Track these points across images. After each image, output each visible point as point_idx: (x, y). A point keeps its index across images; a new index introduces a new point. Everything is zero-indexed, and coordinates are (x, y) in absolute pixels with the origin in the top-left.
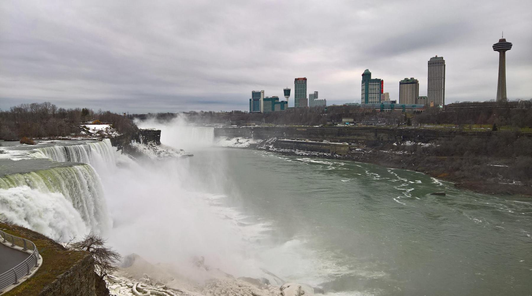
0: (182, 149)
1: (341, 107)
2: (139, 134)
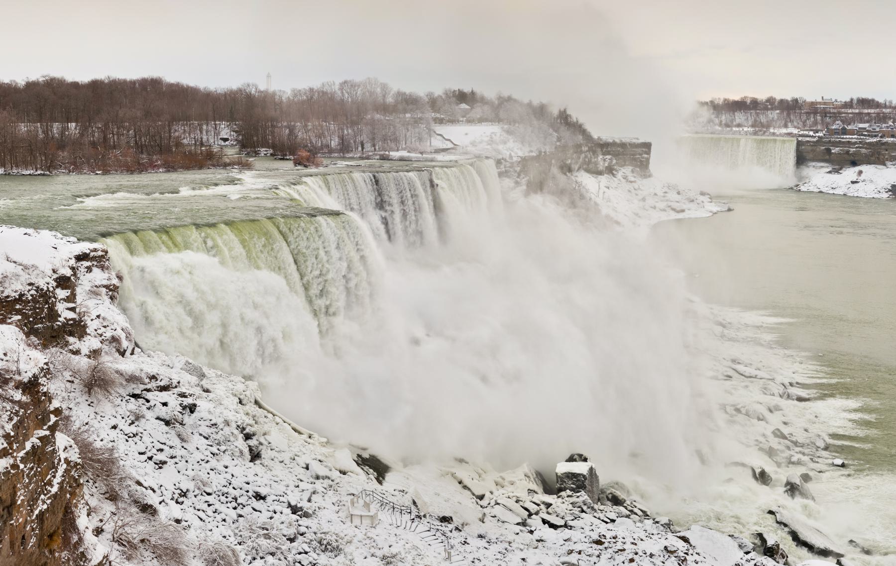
1: (133, 83)
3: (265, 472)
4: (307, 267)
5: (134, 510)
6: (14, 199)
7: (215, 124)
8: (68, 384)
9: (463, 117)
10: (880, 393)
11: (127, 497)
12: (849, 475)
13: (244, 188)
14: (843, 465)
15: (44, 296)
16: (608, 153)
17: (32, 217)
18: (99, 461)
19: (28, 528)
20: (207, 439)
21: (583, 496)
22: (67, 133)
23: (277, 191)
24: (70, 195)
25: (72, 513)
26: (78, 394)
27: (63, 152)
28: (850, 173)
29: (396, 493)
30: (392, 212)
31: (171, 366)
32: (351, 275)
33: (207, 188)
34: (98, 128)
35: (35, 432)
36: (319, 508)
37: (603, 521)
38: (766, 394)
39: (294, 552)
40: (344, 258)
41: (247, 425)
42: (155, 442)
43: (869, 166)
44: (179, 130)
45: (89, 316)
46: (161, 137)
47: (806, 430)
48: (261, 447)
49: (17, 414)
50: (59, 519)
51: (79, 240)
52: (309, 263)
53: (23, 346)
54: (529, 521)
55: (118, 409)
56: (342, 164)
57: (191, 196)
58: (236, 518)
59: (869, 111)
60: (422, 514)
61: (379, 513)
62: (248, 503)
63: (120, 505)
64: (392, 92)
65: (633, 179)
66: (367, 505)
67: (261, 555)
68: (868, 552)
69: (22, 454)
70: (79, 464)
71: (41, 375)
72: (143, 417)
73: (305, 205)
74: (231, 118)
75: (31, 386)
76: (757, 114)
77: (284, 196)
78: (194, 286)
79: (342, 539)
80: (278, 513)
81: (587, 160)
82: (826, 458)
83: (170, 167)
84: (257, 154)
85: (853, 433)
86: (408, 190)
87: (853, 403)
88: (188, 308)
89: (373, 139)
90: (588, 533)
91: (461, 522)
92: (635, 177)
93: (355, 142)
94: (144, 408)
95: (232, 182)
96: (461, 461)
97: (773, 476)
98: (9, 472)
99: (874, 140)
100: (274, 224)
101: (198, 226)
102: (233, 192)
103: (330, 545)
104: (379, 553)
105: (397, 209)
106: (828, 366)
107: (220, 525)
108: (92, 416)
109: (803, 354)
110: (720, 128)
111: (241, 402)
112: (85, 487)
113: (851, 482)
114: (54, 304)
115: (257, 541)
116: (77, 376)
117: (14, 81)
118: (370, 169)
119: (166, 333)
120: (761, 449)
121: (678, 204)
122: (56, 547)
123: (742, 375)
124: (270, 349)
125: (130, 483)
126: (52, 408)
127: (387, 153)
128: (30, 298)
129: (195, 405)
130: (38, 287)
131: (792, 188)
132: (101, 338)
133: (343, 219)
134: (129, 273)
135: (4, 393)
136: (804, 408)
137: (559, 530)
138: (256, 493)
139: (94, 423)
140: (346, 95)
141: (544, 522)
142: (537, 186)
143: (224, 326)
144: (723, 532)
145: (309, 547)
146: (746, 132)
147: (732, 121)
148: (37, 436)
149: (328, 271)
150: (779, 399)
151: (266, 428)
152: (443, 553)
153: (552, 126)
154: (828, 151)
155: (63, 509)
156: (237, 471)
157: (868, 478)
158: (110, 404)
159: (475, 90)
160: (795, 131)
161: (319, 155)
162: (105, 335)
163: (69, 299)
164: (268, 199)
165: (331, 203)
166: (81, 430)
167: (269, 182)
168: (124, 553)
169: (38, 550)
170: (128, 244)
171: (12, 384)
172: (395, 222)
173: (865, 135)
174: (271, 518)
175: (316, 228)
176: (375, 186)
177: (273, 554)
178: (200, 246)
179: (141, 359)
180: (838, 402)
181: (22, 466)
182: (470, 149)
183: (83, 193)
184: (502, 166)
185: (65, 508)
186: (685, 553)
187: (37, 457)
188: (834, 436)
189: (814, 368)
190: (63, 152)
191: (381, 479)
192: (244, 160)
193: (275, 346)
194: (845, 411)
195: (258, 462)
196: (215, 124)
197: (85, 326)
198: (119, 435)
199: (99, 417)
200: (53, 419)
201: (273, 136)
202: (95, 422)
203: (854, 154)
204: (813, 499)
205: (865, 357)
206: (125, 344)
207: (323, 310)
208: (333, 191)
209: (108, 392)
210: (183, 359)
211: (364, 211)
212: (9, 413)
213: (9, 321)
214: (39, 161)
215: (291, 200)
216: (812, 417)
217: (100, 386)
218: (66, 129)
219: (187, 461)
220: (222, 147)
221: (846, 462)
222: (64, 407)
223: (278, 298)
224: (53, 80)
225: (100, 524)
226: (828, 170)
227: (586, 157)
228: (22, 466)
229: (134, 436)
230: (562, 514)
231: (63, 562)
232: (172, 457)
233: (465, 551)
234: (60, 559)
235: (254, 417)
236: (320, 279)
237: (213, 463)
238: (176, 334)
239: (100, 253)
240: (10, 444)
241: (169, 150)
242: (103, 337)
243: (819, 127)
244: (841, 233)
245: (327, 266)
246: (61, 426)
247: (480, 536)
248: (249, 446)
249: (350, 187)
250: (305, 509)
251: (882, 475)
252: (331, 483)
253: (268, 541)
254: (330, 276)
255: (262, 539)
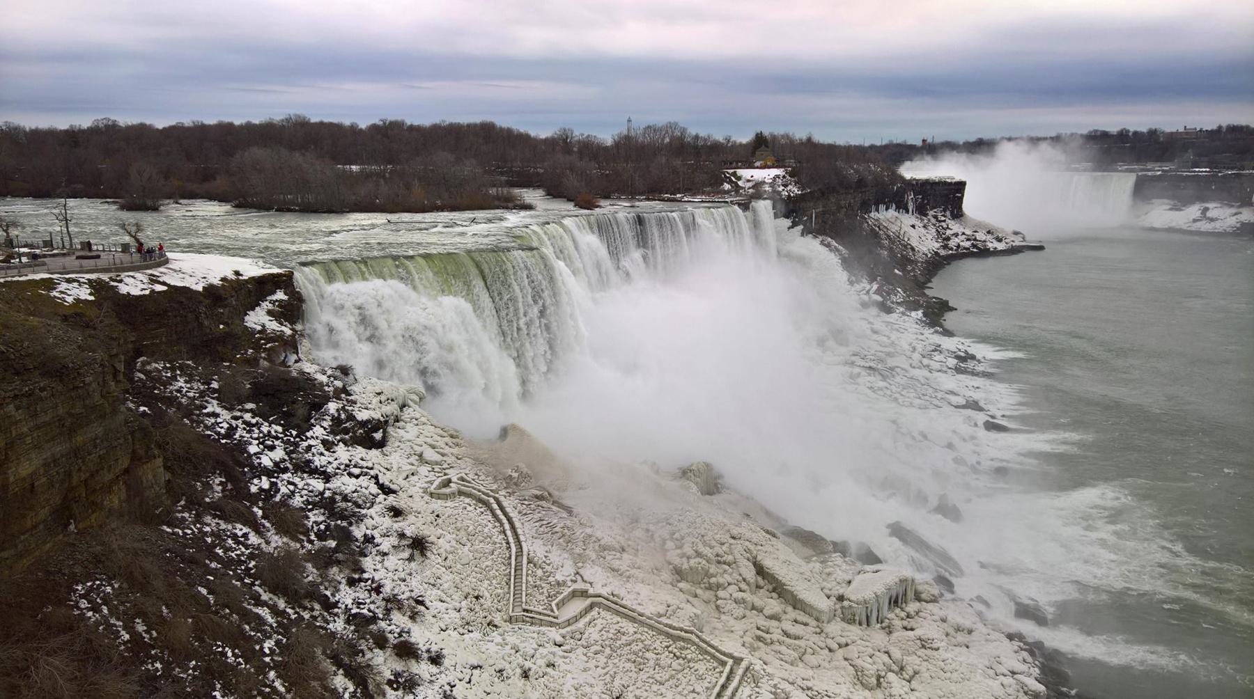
0: (1018, 230)
2: (905, 191)
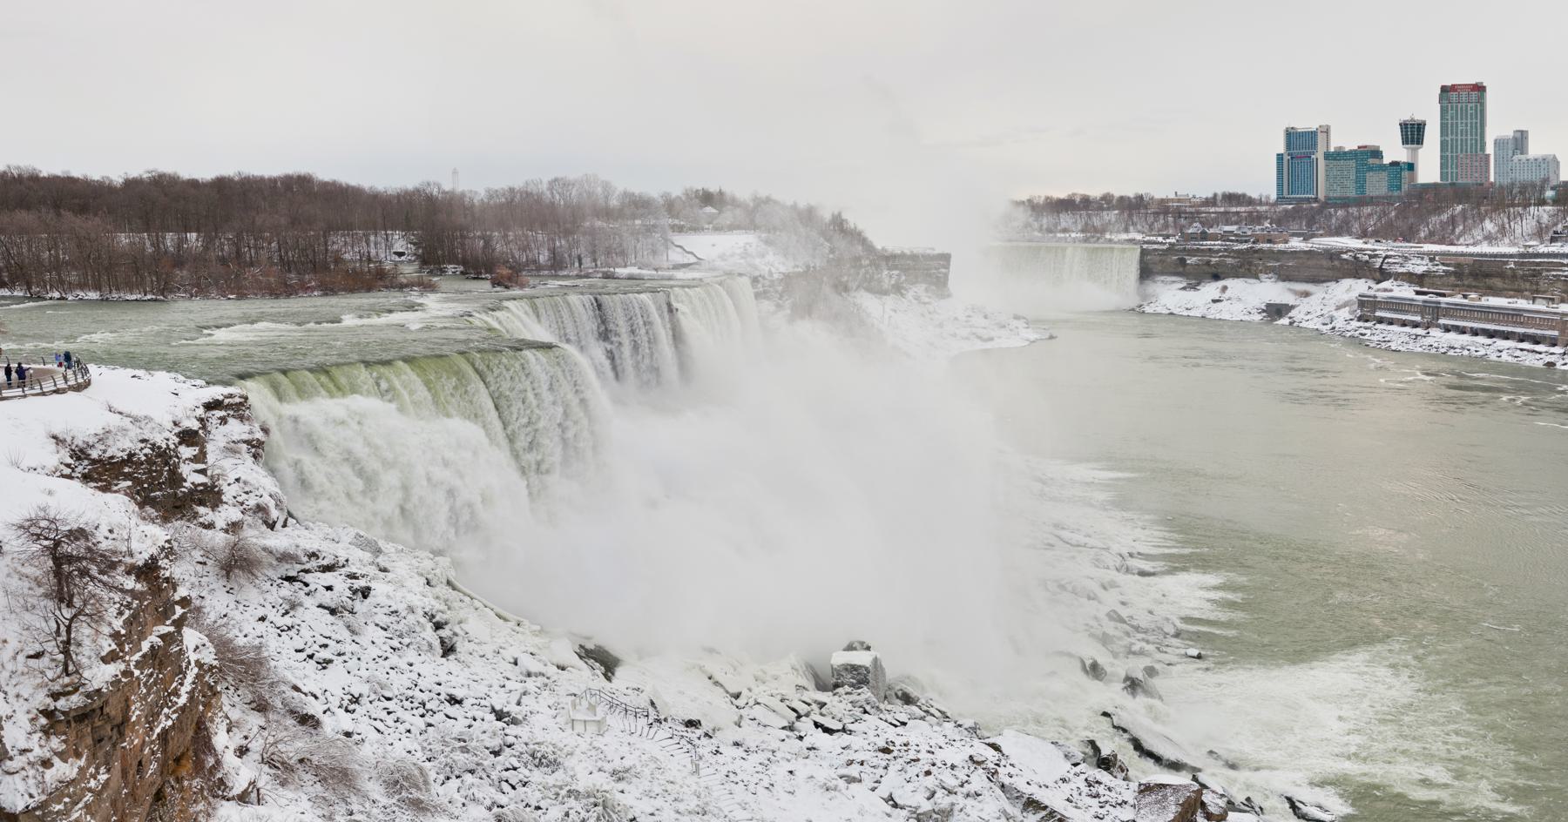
1: (273, 181)
3: (462, 670)
4: (511, 413)
5: (290, 722)
6: (116, 332)
7: (387, 235)
8: (199, 567)
9: (709, 223)
10: (1248, 567)
11: (280, 706)
12: (1207, 669)
13: (428, 316)
14: (1199, 657)
15: (163, 456)
16: (896, 268)
17: (142, 355)
18: (242, 662)
19: (147, 751)
20: (386, 630)
21: (866, 693)
22: (185, 246)
23: (470, 319)
24: (193, 325)
25: (206, 729)
26: (212, 578)
27: (181, 270)
28: (1211, 289)
29: (629, 692)
30: (620, 343)
31: (337, 540)
32: (569, 423)
33: (379, 316)
34: (228, 239)
35: (155, 628)
36: (531, 713)
37: (891, 724)
38: (1098, 567)
39: (499, 768)
40: (560, 402)
41: (437, 611)
42: (318, 636)
43: (1237, 281)
44: (337, 242)
45: (225, 480)
46: (314, 251)
47: (1151, 612)
48: (455, 639)
49: (129, 606)
50: (189, 738)
51: (208, 383)
52: (514, 409)
53: (135, 519)
54: (797, 724)
55: (267, 596)
56: (554, 284)
57: (357, 326)
58: (423, 728)
59: (1238, 209)
60: (662, 717)
61: (608, 717)
62: (440, 708)
63: (271, 716)
64: (617, 193)
65: (927, 300)
66: (592, 708)
67: (457, 773)
68: (1233, 767)
69: (137, 657)
70: (215, 667)
71: (162, 556)
72: (301, 605)
73: (508, 336)
74: (406, 226)
75: (148, 571)
76: (1089, 216)
77: (480, 325)
78: (365, 439)
79: (561, 750)
80: (479, 720)
81: (868, 276)
82: (1178, 648)
83: (328, 290)
84: (442, 272)
85: (1212, 617)
86: (639, 316)
87: (1212, 579)
88: (357, 467)
89: (594, 252)
90: (873, 739)
91: (712, 726)
92: (930, 297)
93: (570, 256)
94: (302, 593)
95: (411, 307)
96: (711, 651)
97: (1108, 669)
98: (120, 681)
99: (1245, 246)
100: (468, 360)
101: (367, 364)
102: (413, 320)
103: (545, 758)
104: (609, 767)
105: (626, 339)
106: (1180, 532)
107: (403, 737)
108: (232, 605)
109: (1147, 517)
110: (1040, 235)
111: (428, 583)
112: (224, 696)
113: (1211, 678)
114: (176, 466)
115: (451, 755)
116: (211, 556)
117: (108, 178)
118: (590, 291)
119: (329, 499)
120: (1092, 635)
121: (985, 331)
122: (184, 774)
123: (1068, 543)
124: (465, 517)
125: (283, 688)
126: (177, 597)
127: (612, 269)
128: (143, 458)
129: (369, 589)
130: (154, 445)
131: (1133, 310)
132: (242, 508)
133: (557, 354)
134: (278, 424)
135: (110, 580)
136: (1149, 585)
137: (836, 735)
138: (450, 696)
139: (236, 615)
140: (557, 197)
141: (817, 725)
142: (805, 310)
143: (406, 488)
144: (1044, 739)
145: (519, 762)
146: (1074, 238)
147: (1056, 225)
148: (157, 634)
149: (539, 418)
150: (1115, 572)
151: (462, 614)
152: (689, 766)
153: (823, 233)
154: (1182, 262)
155: (194, 724)
156: (426, 670)
157: (1232, 672)
158: (255, 590)
159: (723, 190)
160: (1139, 237)
161: (524, 273)
162: (247, 503)
163: (195, 459)
164: (459, 329)
165: (542, 334)
166: (218, 624)
167: (460, 308)
168: (277, 777)
169: (160, 779)
170: (276, 389)
171: (121, 569)
172: (623, 356)
173: (1232, 241)
174: (470, 727)
175: (522, 364)
176: (597, 312)
177: (472, 772)
178: (371, 388)
179: (297, 532)
180: (1193, 578)
181: (137, 673)
182: (719, 263)
183: (211, 323)
184: (760, 285)
185: (197, 723)
186: (996, 764)
187: (158, 660)
188: (1187, 620)
189: (1161, 534)
190: (181, 270)
191: (610, 674)
192: (426, 279)
193: (472, 514)
194: (1201, 588)
195: (452, 657)
196: (387, 235)
197: (220, 493)
198: (270, 629)
199: (241, 607)
200: (179, 611)
201: (463, 249)
202: (237, 613)
203: (1217, 264)
204: (1160, 698)
205: (1229, 521)
206: (274, 514)
207: (534, 467)
208: (543, 320)
209: (253, 574)
210: (352, 532)
211: (583, 343)
212: (118, 606)
213: (115, 488)
214: (148, 283)
215: (489, 330)
216: (1159, 596)
217: (241, 568)
218: (181, 241)
219: (359, 659)
220: (396, 264)
221: (1203, 653)
222: (194, 594)
223: (475, 453)
224: (162, 176)
225: (244, 742)
226: (1182, 286)
227: (867, 272)
228: (137, 673)
229: (289, 629)
230: (840, 716)
231: (195, 793)
232: (339, 655)
233: (717, 763)
234: (191, 788)
235: (446, 601)
236: (529, 429)
237: (394, 659)
238: (343, 500)
239: (237, 400)
240: (121, 645)
241: (327, 268)
242: (244, 506)
243: (1171, 231)
244: (1198, 365)
245: (538, 412)
246: (190, 620)
247: (737, 744)
248: (440, 638)
249: (565, 314)
250: (513, 715)
251: (1251, 669)
252: (546, 681)
253: (466, 755)
254: (541, 425)
255: (458, 753)
